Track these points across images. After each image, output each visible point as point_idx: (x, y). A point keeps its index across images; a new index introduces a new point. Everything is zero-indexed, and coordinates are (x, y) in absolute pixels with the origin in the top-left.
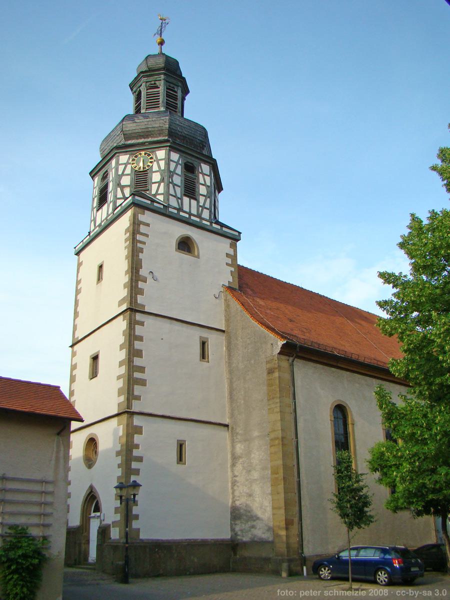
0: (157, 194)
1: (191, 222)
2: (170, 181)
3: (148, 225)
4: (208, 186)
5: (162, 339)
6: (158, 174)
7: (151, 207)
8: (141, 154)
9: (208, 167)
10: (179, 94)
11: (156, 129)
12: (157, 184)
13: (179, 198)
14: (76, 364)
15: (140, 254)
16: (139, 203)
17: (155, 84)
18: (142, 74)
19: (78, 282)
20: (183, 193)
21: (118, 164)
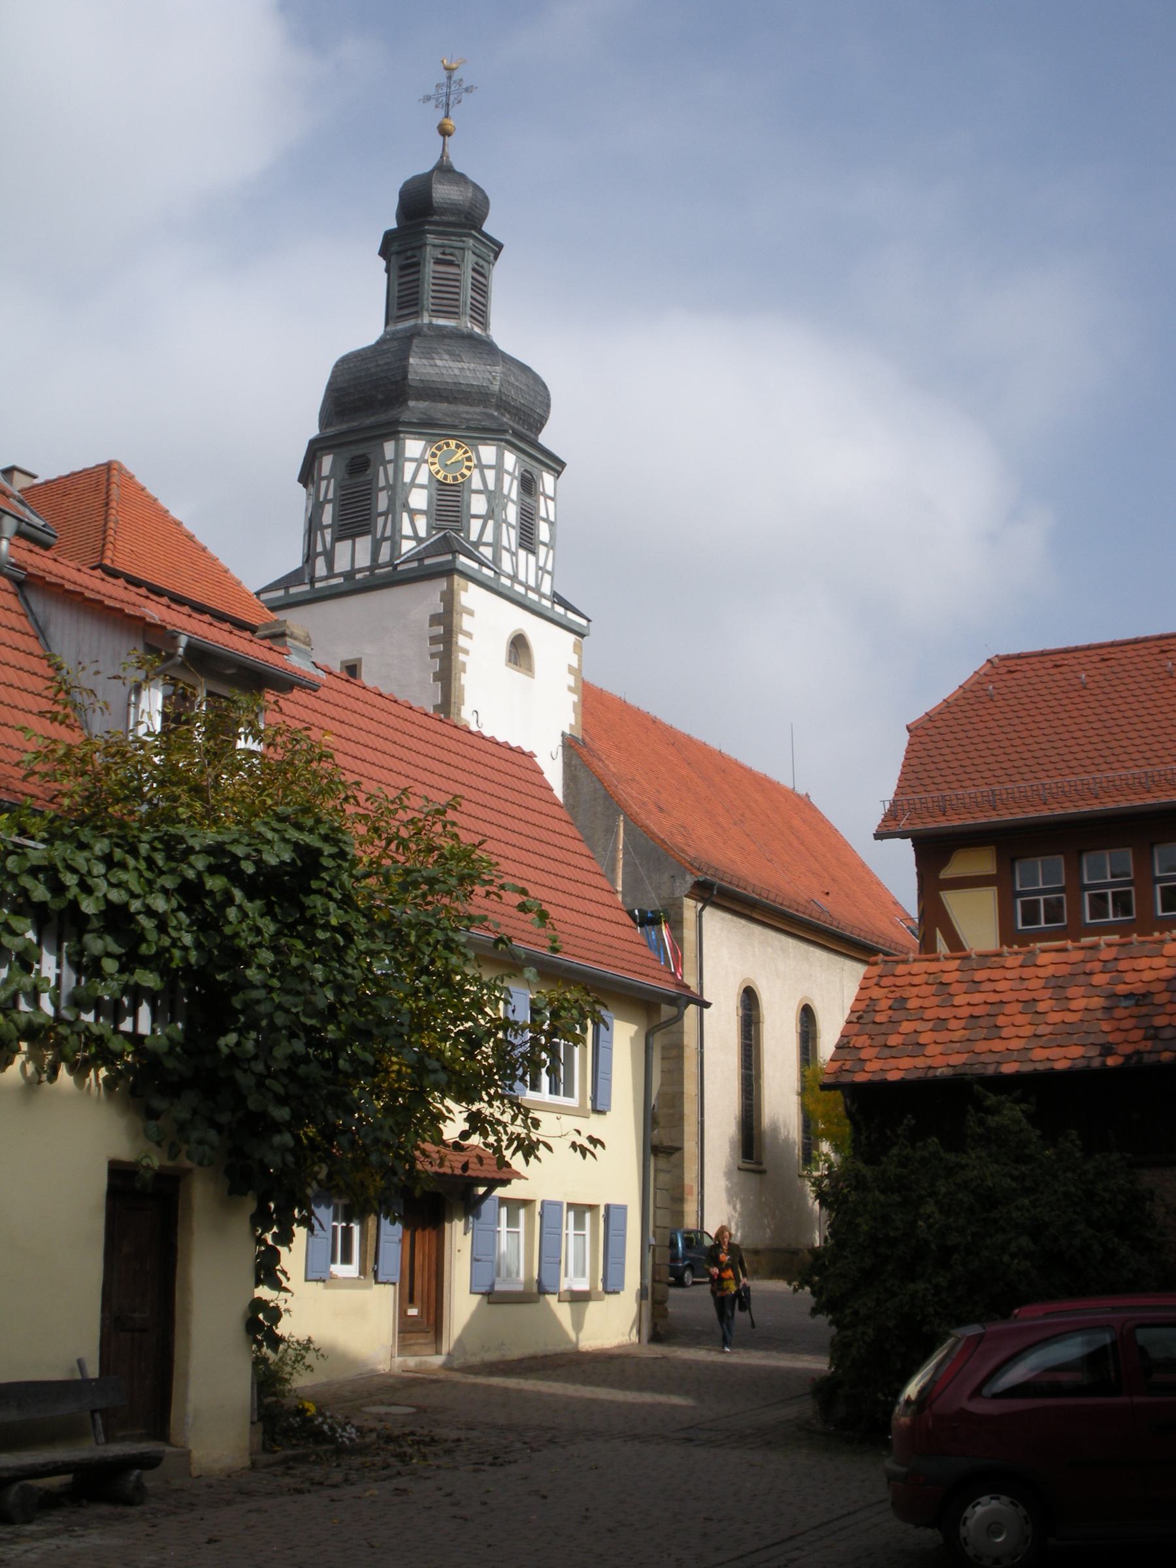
8: (448, 445)
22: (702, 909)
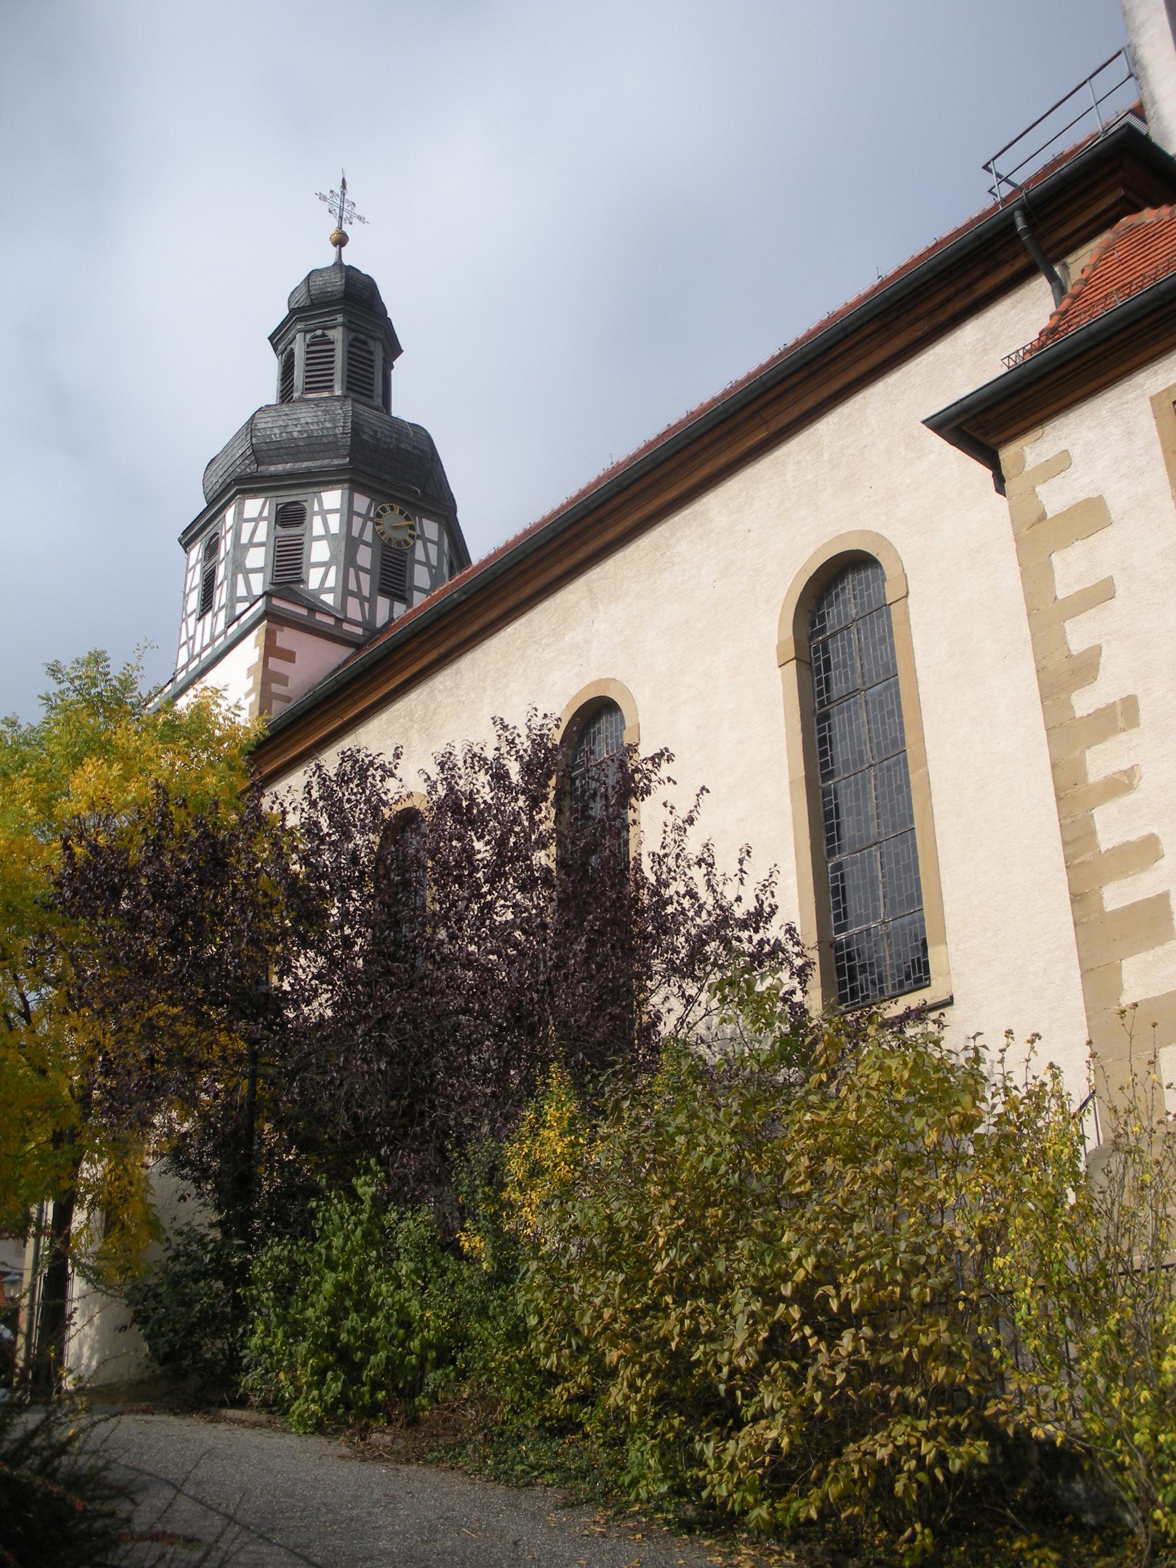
0: (322, 589)
10: (378, 357)
17: (324, 335)
18: (297, 314)
20: (377, 584)
21: (240, 518)
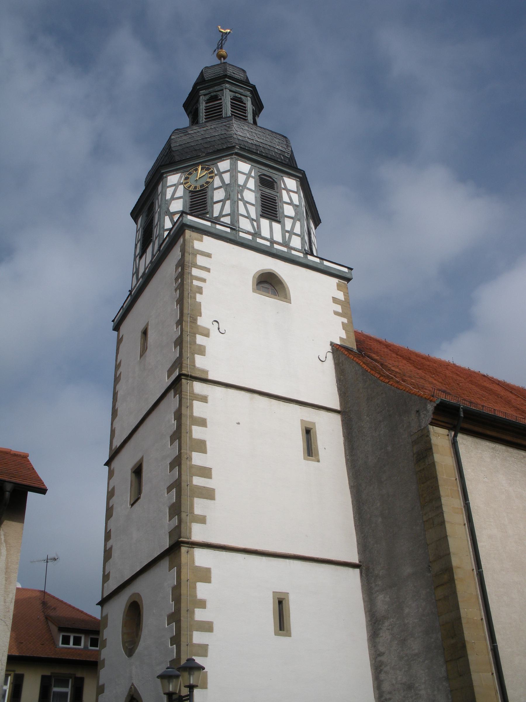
0: (221, 215)
1: (275, 252)
2: (240, 197)
3: (209, 255)
4: (296, 206)
5: (238, 423)
6: (222, 190)
7: (213, 230)
9: (295, 181)
11: (218, 138)
12: (224, 213)
13: (253, 220)
14: (113, 488)
15: (198, 295)
16: (192, 224)
19: (117, 367)
22: (455, 436)
